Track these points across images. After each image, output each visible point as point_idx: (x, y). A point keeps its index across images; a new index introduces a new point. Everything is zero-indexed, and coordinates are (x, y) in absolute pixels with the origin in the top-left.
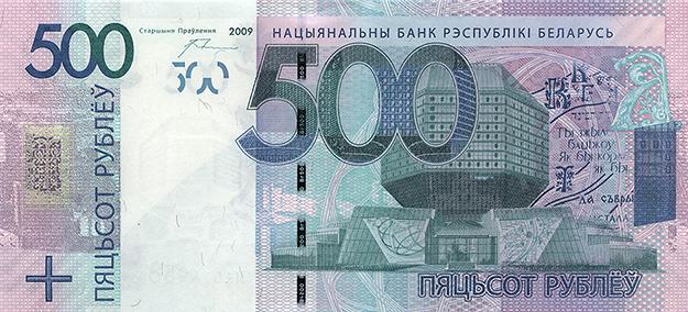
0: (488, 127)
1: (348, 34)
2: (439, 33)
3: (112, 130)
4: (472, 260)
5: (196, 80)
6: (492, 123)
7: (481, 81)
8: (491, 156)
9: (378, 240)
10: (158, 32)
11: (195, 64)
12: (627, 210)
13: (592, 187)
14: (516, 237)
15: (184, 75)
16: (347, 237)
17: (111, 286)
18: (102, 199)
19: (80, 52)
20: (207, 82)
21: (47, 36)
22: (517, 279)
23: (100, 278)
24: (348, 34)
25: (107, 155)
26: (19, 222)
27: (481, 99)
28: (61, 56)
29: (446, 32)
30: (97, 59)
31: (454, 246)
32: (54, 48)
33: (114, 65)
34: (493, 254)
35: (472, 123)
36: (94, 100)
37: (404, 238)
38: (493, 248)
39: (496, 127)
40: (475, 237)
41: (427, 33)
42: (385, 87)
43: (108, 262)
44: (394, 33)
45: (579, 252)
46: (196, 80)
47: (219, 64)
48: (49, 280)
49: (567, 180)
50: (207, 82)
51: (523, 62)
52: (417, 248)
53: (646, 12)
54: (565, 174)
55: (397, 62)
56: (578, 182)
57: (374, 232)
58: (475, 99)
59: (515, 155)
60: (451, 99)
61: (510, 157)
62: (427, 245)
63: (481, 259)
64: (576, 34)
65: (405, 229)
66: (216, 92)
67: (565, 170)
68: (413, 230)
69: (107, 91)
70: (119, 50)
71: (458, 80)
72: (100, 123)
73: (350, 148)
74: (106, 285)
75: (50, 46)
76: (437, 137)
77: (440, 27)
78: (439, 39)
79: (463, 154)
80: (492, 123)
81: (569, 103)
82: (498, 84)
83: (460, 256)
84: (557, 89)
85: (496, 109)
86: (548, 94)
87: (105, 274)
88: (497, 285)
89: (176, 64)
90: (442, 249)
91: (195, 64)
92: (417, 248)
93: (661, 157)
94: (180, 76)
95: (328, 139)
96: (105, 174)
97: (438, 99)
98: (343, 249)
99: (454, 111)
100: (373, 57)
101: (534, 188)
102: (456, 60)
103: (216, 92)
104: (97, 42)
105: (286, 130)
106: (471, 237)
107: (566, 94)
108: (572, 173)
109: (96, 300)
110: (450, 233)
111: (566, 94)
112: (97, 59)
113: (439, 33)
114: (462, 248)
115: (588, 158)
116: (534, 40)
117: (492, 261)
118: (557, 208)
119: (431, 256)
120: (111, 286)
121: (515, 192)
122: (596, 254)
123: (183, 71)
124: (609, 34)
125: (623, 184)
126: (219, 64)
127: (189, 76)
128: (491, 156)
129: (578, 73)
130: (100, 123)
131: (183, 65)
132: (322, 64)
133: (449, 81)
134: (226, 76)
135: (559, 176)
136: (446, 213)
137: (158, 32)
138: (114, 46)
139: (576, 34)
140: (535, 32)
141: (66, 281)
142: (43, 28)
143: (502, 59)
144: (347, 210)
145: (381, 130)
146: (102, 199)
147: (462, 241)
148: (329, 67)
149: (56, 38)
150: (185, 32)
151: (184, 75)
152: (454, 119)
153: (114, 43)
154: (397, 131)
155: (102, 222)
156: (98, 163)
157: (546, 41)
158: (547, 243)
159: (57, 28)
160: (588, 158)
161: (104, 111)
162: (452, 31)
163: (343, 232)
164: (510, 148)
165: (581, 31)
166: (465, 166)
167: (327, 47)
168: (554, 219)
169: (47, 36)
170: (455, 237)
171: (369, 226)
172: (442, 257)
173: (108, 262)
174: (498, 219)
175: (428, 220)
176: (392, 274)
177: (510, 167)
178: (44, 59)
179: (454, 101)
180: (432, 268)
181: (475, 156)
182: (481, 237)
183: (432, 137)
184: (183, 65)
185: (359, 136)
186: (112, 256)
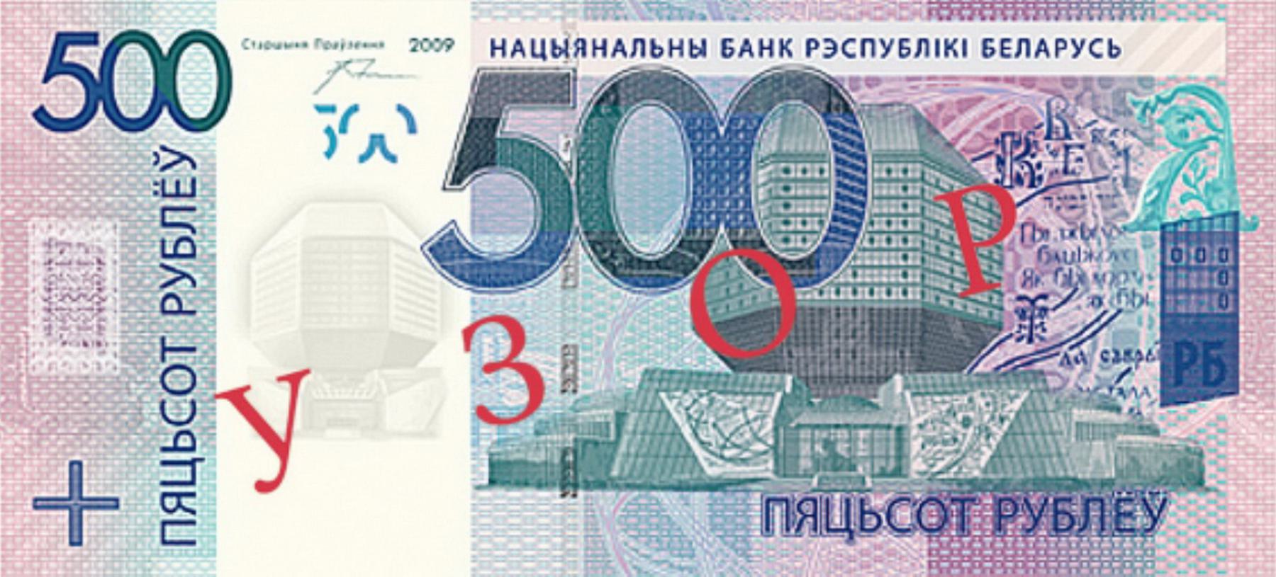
0: (889, 223)
1: (629, 49)
2: (798, 47)
3: (194, 231)
4: (860, 470)
5: (353, 142)
6: (898, 215)
7: (875, 140)
8: (895, 277)
9: (687, 431)
10: (287, 46)
11: (355, 109)
12: (1149, 375)
13: (1089, 332)
14: (941, 429)
15: (336, 129)
16: (629, 427)
17: (189, 517)
18: (172, 358)
19: (133, 85)
20: (377, 141)
21: (73, 54)
22: (947, 510)
23: (171, 502)
24: (629, 49)
25: (185, 275)
26: (30, 402)
27: (875, 171)
28: (100, 91)
29: (811, 45)
30: (165, 98)
31: (828, 444)
32: (91, 79)
33: (197, 106)
34: (899, 457)
35: (861, 215)
36: (157, 174)
37: (742, 423)
38: (899, 448)
39: (905, 241)
40: (865, 426)
41: (589, 48)
42: (699, 149)
43: (184, 473)
44: (714, 48)
45: (1059, 455)
46: (353, 142)
47: (401, 109)
48: (76, 504)
49: (1037, 321)
50: (377, 141)
51: (965, 105)
52: (760, 447)
53: (94, 212)
54: (1032, 311)
55: (722, 106)
56: (1056, 325)
57: (679, 419)
58: (865, 171)
59: (942, 274)
60: (822, 171)
61: (931, 280)
62: (777, 441)
63: (877, 470)
64: (1052, 49)
65: (736, 411)
66: (393, 159)
67: (1033, 302)
68: (751, 414)
69: (184, 157)
70: (184, 79)
71: (834, 135)
72: (170, 217)
73: (634, 262)
74: (179, 515)
75: (79, 72)
76: (796, 242)
77: (800, 35)
78: (798, 60)
79: (843, 275)
80: (898, 215)
81: (1040, 178)
82: (908, 140)
83: (836, 462)
84: (1017, 152)
85: (905, 188)
86: (1000, 162)
87: (179, 495)
88: (904, 515)
89: (321, 109)
90: (805, 449)
91: (355, 109)
92: (760, 447)
93: (1211, 279)
94: (329, 131)
95: (593, 244)
96: (180, 311)
97: (796, 171)
98: (623, 448)
99: (826, 192)
100: (678, 95)
101: (980, 336)
102: (831, 99)
103: (393, 159)
104: (166, 65)
105: (516, 231)
106: (856, 427)
107: (1034, 162)
108: (1044, 310)
109: (164, 542)
110: (818, 419)
111: (1034, 162)
112: (165, 98)
113: (798, 47)
114: (841, 449)
115: (1074, 284)
116: (974, 65)
117: (898, 472)
118: (1017, 370)
119: (784, 459)
120: (189, 517)
121: (936, 343)
122: (1096, 461)
123: (334, 120)
124: (1114, 51)
125: (1146, 331)
126: (401, 109)
127: (343, 130)
128: (895, 277)
129: (1057, 122)
130: (170, 217)
131: (332, 109)
132: (580, 108)
133: (816, 135)
134: (412, 129)
135: (1022, 314)
136: (815, 384)
137: (287, 46)
138: (195, 81)
139: (1052, 49)
140: (975, 48)
141: (71, 536)
142: (63, 41)
143: (925, 101)
144: (632, 377)
145: (691, 229)
146: (172, 358)
147: (842, 434)
148: (596, 112)
149: (90, 58)
150: (327, 46)
151: (336, 129)
152: (827, 208)
153: (196, 62)
154: (722, 230)
155: (171, 400)
156: (169, 290)
157: (997, 66)
158: (999, 438)
159: (91, 39)
160: (1074, 284)
161: (178, 195)
162: (823, 45)
163: (620, 417)
164: (932, 263)
165: (811, 45)
166: (846, 294)
167: (596, 71)
168: (1012, 392)
169: (73, 54)
170: (828, 426)
171: (671, 406)
172: (805, 463)
173: (184, 473)
174: (908, 394)
175: (779, 395)
176: (718, 494)
177: (930, 298)
178: (67, 97)
179: (826, 175)
180: (787, 483)
181: (864, 277)
182: (876, 426)
183: (786, 240)
184: (332, 109)
185: (652, 242)
186: (192, 463)
